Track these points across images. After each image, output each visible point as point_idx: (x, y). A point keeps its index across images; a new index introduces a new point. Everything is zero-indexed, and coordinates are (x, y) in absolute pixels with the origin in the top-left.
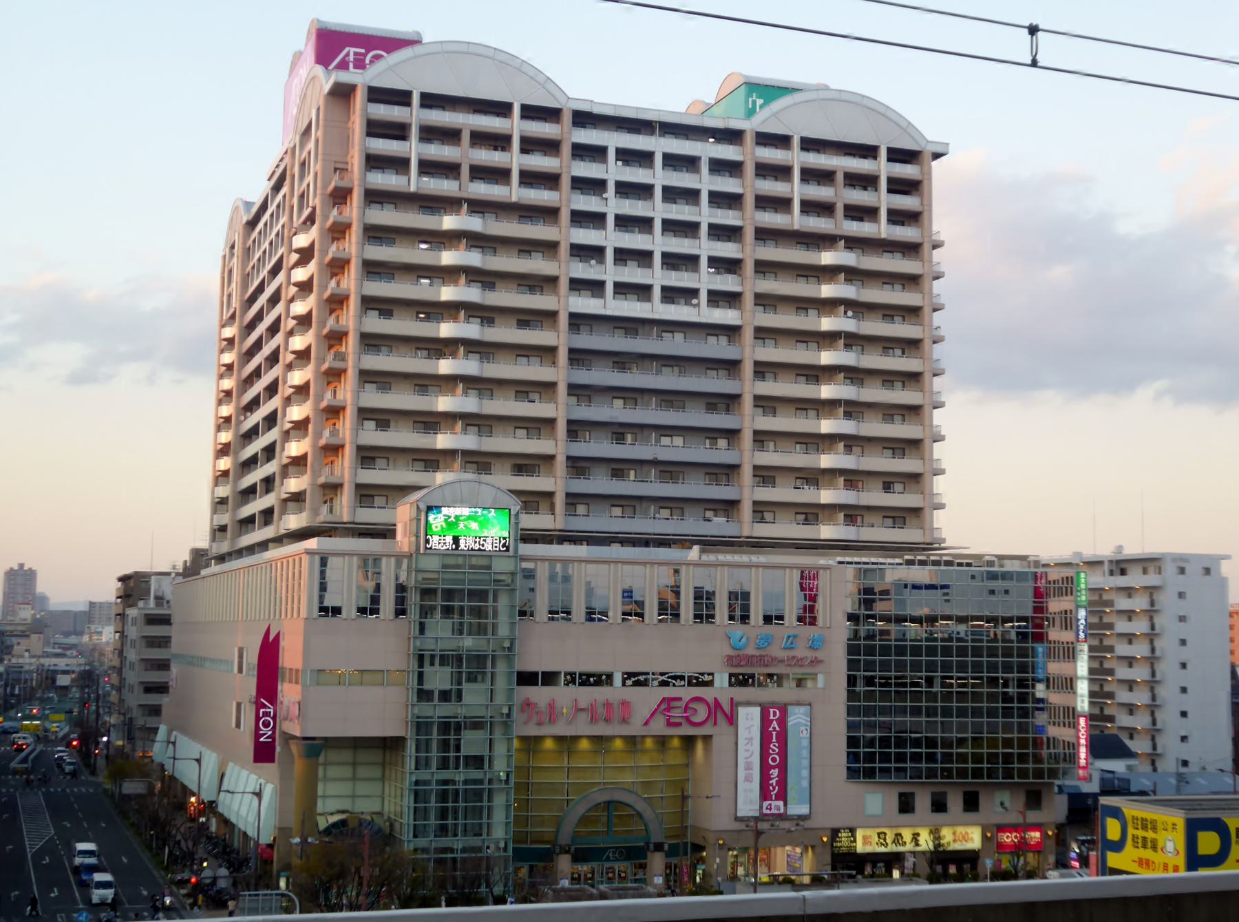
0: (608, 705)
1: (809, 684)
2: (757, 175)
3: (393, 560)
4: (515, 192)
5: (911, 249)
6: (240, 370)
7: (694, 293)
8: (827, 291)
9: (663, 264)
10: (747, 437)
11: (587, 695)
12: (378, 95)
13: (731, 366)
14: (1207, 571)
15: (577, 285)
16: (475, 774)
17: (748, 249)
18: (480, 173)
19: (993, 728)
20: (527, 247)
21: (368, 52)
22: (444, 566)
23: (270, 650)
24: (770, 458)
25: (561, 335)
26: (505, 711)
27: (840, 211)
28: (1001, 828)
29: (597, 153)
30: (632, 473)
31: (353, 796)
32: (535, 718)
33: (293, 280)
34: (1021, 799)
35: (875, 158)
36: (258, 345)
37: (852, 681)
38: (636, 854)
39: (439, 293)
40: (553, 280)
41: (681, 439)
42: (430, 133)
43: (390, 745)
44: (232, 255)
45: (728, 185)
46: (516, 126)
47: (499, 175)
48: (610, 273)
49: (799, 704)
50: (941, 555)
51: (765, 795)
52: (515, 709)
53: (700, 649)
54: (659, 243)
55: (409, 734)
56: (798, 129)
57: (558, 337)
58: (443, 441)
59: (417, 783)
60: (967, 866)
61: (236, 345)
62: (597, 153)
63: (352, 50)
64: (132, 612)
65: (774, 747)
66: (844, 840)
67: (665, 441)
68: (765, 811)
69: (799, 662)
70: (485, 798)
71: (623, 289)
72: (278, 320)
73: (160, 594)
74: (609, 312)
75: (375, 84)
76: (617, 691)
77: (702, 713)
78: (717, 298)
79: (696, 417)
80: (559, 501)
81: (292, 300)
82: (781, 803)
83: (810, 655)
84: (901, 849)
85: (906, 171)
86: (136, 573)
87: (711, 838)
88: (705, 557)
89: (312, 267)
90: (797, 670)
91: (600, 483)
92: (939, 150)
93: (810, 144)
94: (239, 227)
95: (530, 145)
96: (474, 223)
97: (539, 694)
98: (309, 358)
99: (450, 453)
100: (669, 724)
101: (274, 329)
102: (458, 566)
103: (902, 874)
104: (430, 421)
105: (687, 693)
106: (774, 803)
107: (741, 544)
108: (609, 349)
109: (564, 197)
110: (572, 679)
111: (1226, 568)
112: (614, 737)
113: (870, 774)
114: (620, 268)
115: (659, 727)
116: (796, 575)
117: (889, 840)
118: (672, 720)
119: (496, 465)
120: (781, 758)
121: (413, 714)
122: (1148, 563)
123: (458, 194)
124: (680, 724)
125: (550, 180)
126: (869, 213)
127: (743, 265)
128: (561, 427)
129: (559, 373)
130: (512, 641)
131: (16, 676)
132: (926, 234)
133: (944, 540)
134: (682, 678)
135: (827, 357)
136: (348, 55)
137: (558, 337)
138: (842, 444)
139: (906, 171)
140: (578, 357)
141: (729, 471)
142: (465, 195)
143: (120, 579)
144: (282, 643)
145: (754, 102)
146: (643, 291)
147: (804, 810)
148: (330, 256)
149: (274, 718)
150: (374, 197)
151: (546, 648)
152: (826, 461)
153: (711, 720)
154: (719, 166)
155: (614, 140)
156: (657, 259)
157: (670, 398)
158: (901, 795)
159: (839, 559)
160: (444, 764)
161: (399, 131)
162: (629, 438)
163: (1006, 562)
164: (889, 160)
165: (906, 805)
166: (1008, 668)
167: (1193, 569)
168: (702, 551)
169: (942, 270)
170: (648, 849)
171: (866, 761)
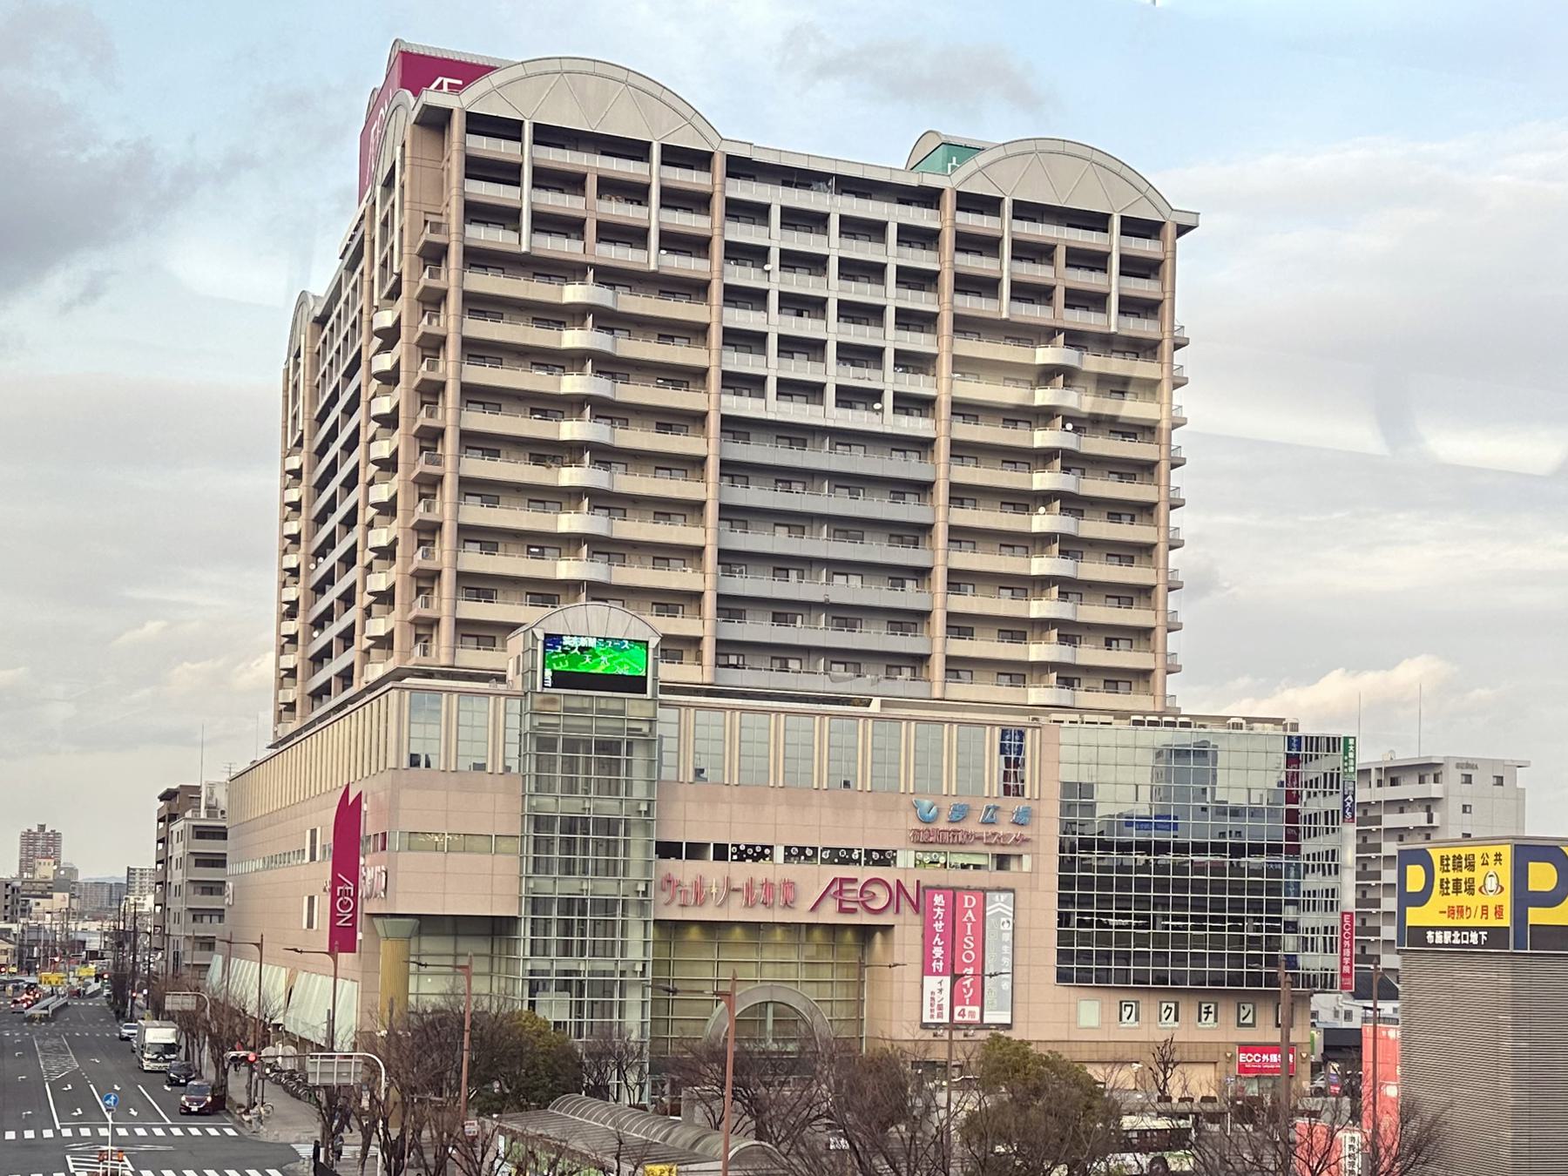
0: (767, 885)
1: (1014, 864)
2: (956, 290)
4: (652, 259)
6: (309, 541)
7: (877, 395)
9: (838, 358)
10: (940, 577)
11: (742, 872)
12: (478, 124)
16: (603, 964)
17: (945, 341)
18: (611, 232)
20: (668, 330)
23: (349, 813)
24: (968, 517)
25: (711, 442)
26: (644, 807)
27: (591, 229)
32: (678, 900)
33: (372, 500)
36: (331, 507)
37: (1064, 919)
39: (559, 384)
42: (546, 178)
43: (498, 929)
44: (297, 365)
45: (920, 259)
46: (654, 173)
48: (772, 366)
49: (999, 890)
52: (652, 886)
54: (832, 330)
55: (525, 913)
56: (531, 110)
57: (707, 445)
59: (532, 972)
61: (303, 543)
62: (758, 213)
64: (177, 827)
68: (957, 1018)
70: (619, 911)
71: (788, 388)
73: (213, 803)
76: (775, 870)
77: (882, 899)
80: (708, 649)
81: (371, 483)
83: (1015, 832)
89: (400, 393)
91: (757, 629)
92: (1186, 222)
93: (1023, 211)
94: (307, 324)
96: (601, 296)
97: (674, 867)
98: (393, 558)
100: (842, 910)
101: (350, 521)
102: (583, 710)
105: (863, 873)
106: (968, 1009)
109: (717, 224)
113: (1084, 978)
114: (786, 361)
115: (829, 914)
121: (527, 889)
122: (1426, 770)
124: (853, 911)
125: (697, 245)
126: (1096, 301)
127: (933, 576)
129: (708, 489)
131: (33, 936)
137: (707, 445)
138: (1056, 589)
139: (1141, 288)
141: (918, 532)
143: (162, 798)
146: (813, 391)
148: (418, 470)
149: (355, 898)
150: (477, 258)
153: (892, 909)
154: (908, 235)
155: (777, 196)
156: (831, 350)
160: (566, 949)
161: (508, 173)
163: (1256, 725)
171: (1076, 968)
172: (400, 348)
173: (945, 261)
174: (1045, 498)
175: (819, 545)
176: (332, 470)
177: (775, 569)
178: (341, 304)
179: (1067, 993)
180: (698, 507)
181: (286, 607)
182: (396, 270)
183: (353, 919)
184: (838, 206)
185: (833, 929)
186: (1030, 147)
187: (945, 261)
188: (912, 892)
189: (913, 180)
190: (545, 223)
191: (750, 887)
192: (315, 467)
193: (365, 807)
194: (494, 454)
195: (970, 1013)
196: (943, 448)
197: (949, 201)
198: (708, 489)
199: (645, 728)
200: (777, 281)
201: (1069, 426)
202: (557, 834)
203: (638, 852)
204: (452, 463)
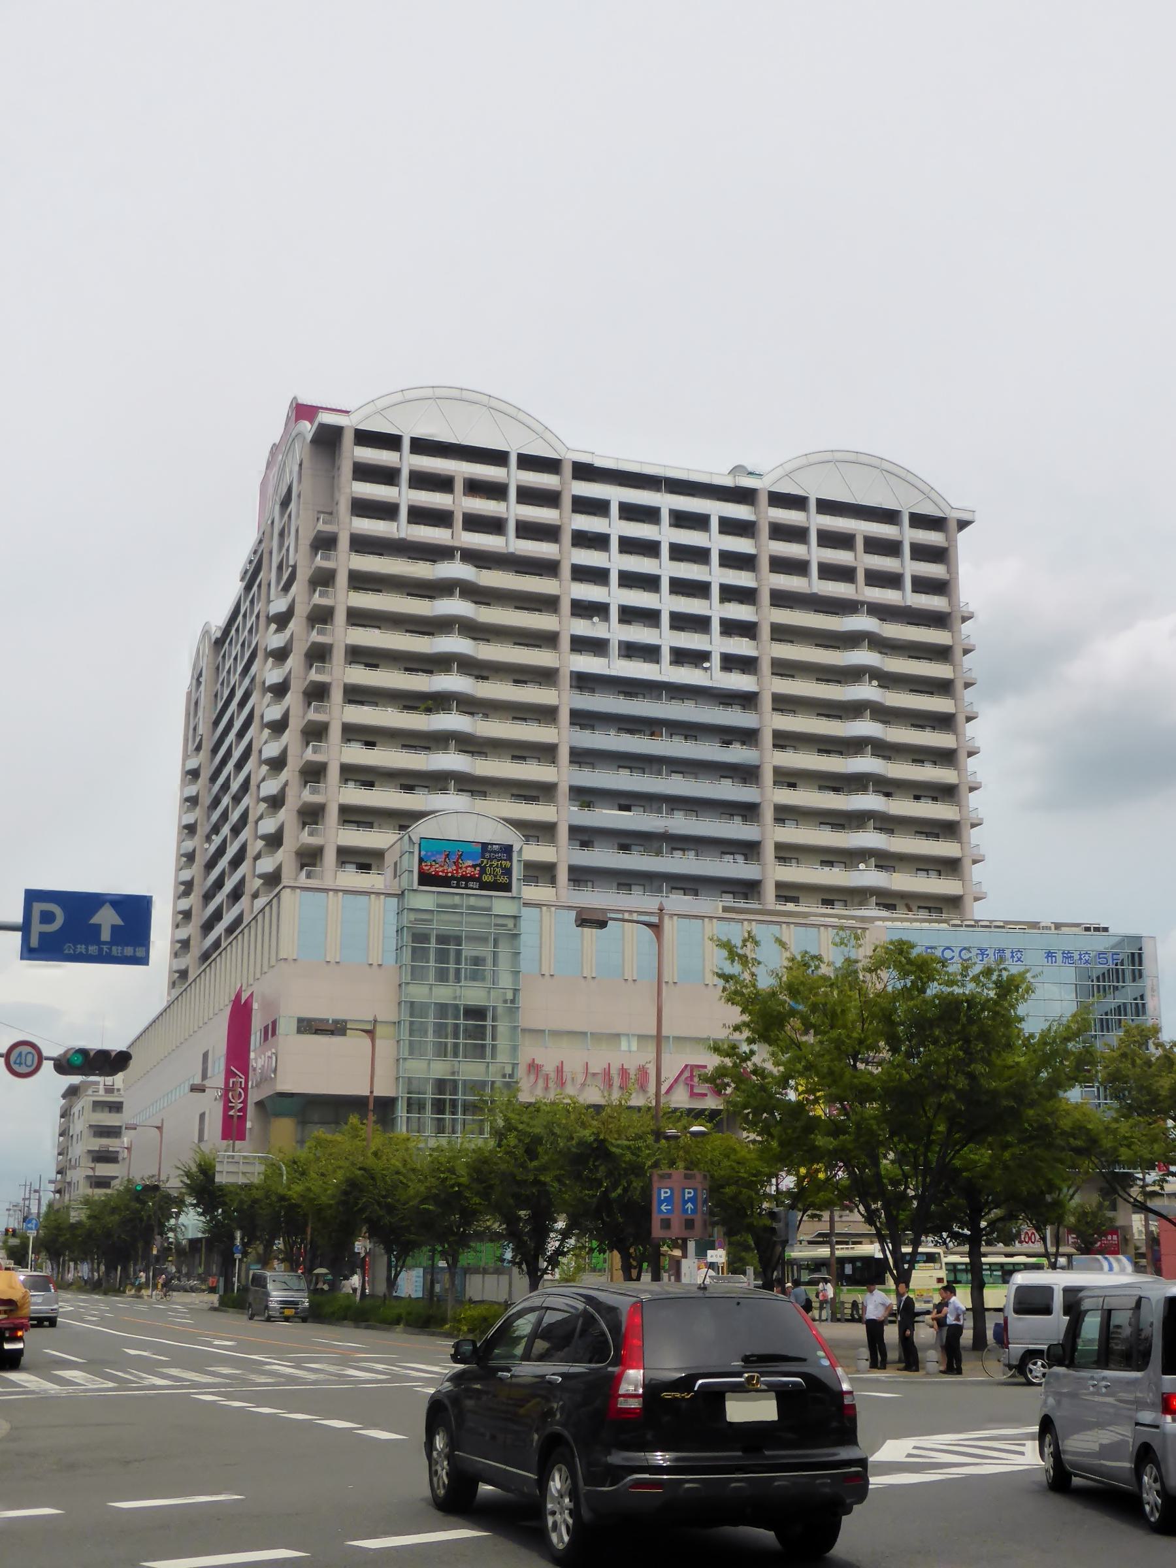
18: (474, 523)
26: (510, 996)
27: (860, 576)
29: (598, 507)
33: (260, 832)
42: (421, 480)
44: (199, 683)
47: (495, 526)
62: (598, 507)
72: (242, 881)
75: (360, 427)
78: (731, 662)
85: (932, 538)
92: (965, 516)
95: (528, 496)
102: (455, 906)
108: (620, 711)
118: (696, 1091)
123: (450, 543)
124: (705, 1095)
125: (549, 533)
139: (932, 538)
146: (650, 653)
150: (362, 544)
154: (730, 527)
155: (615, 494)
169: (982, 852)
172: (285, 775)
176: (219, 884)
177: (619, 884)
178: (240, 618)
181: (182, 887)
182: (291, 563)
184: (666, 502)
186: (828, 456)
189: (728, 482)
190: (419, 515)
191: (607, 1073)
192: (205, 879)
193: (255, 1006)
194: (370, 785)
197: (763, 499)
199: (510, 923)
200: (616, 596)
201: (875, 683)
202: (432, 964)
204: (344, 598)
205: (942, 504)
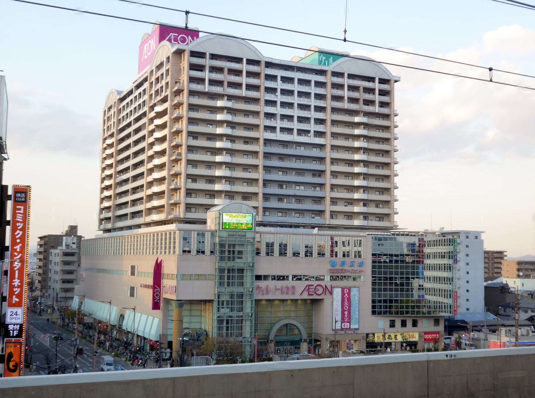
0: (287, 288)
1: (358, 280)
3: (210, 233)
4: (244, 92)
5: (386, 116)
7: (309, 132)
8: (357, 132)
11: (280, 284)
12: (193, 54)
13: (322, 160)
14: (476, 237)
15: (267, 128)
17: (329, 115)
18: (231, 85)
19: (396, 296)
20: (247, 113)
21: (179, 35)
22: (229, 235)
27: (226, 84)
28: (426, 333)
30: (285, 200)
31: (190, 322)
32: (261, 293)
34: (432, 322)
35: (374, 82)
38: (296, 344)
40: (257, 126)
41: (303, 187)
42: (213, 69)
47: (238, 85)
49: (354, 287)
50: (400, 232)
51: (343, 321)
52: (254, 290)
53: (320, 267)
56: (209, 50)
57: (259, 148)
58: (218, 187)
59: (218, 317)
60: (413, 347)
63: (173, 34)
65: (346, 303)
66: (371, 338)
67: (298, 188)
68: (343, 327)
69: (355, 272)
71: (283, 130)
73: (67, 244)
74: (278, 139)
76: (290, 283)
77: (320, 291)
79: (308, 178)
82: (348, 324)
83: (359, 269)
84: (390, 341)
86: (49, 235)
87: (324, 337)
88: (319, 232)
90: (354, 274)
92: (396, 79)
93: (351, 76)
95: (250, 74)
96: (229, 104)
97: (263, 284)
99: (220, 192)
100: (309, 295)
102: (233, 235)
103: (391, 350)
104: (211, 180)
106: (346, 324)
107: (325, 227)
108: (278, 153)
110: (274, 278)
111: (483, 237)
112: (275, 300)
115: (305, 296)
116: (329, 237)
117: (386, 338)
118: (310, 293)
119: (236, 197)
120: (350, 307)
124: (313, 295)
125: (256, 88)
128: (261, 182)
129: (260, 161)
130: (253, 264)
132: (392, 111)
133: (398, 226)
134: (313, 277)
135: (357, 157)
136: (171, 36)
137: (259, 148)
139: (385, 99)
140: (267, 155)
142: (226, 93)
143: (39, 238)
144: (163, 264)
145: (322, 58)
146: (290, 131)
147: (357, 327)
150: (192, 93)
151: (267, 266)
152: (356, 196)
157: (300, 171)
158: (402, 320)
159: (368, 233)
162: (284, 186)
164: (379, 83)
165: (392, 325)
166: (396, 273)
167: (472, 237)
168: (319, 230)
170: (301, 341)
173: (329, 91)
174: (358, 162)
175: (292, 177)
179: (375, 318)
180: (256, 166)
183: (159, 300)
185: (305, 300)
187: (329, 91)
188: (330, 289)
191: (282, 288)
195: (347, 325)
196: (328, 147)
197: (329, 74)
198: (260, 161)
203: (248, 277)
205: (390, 75)
